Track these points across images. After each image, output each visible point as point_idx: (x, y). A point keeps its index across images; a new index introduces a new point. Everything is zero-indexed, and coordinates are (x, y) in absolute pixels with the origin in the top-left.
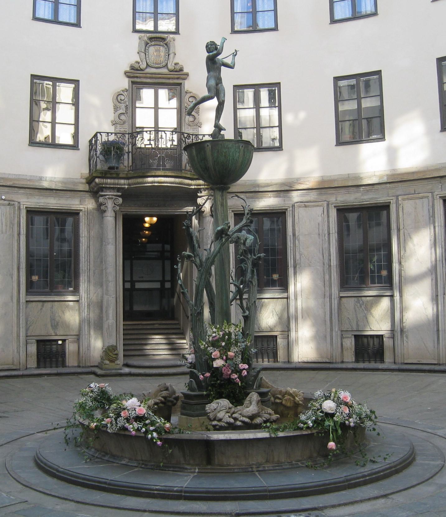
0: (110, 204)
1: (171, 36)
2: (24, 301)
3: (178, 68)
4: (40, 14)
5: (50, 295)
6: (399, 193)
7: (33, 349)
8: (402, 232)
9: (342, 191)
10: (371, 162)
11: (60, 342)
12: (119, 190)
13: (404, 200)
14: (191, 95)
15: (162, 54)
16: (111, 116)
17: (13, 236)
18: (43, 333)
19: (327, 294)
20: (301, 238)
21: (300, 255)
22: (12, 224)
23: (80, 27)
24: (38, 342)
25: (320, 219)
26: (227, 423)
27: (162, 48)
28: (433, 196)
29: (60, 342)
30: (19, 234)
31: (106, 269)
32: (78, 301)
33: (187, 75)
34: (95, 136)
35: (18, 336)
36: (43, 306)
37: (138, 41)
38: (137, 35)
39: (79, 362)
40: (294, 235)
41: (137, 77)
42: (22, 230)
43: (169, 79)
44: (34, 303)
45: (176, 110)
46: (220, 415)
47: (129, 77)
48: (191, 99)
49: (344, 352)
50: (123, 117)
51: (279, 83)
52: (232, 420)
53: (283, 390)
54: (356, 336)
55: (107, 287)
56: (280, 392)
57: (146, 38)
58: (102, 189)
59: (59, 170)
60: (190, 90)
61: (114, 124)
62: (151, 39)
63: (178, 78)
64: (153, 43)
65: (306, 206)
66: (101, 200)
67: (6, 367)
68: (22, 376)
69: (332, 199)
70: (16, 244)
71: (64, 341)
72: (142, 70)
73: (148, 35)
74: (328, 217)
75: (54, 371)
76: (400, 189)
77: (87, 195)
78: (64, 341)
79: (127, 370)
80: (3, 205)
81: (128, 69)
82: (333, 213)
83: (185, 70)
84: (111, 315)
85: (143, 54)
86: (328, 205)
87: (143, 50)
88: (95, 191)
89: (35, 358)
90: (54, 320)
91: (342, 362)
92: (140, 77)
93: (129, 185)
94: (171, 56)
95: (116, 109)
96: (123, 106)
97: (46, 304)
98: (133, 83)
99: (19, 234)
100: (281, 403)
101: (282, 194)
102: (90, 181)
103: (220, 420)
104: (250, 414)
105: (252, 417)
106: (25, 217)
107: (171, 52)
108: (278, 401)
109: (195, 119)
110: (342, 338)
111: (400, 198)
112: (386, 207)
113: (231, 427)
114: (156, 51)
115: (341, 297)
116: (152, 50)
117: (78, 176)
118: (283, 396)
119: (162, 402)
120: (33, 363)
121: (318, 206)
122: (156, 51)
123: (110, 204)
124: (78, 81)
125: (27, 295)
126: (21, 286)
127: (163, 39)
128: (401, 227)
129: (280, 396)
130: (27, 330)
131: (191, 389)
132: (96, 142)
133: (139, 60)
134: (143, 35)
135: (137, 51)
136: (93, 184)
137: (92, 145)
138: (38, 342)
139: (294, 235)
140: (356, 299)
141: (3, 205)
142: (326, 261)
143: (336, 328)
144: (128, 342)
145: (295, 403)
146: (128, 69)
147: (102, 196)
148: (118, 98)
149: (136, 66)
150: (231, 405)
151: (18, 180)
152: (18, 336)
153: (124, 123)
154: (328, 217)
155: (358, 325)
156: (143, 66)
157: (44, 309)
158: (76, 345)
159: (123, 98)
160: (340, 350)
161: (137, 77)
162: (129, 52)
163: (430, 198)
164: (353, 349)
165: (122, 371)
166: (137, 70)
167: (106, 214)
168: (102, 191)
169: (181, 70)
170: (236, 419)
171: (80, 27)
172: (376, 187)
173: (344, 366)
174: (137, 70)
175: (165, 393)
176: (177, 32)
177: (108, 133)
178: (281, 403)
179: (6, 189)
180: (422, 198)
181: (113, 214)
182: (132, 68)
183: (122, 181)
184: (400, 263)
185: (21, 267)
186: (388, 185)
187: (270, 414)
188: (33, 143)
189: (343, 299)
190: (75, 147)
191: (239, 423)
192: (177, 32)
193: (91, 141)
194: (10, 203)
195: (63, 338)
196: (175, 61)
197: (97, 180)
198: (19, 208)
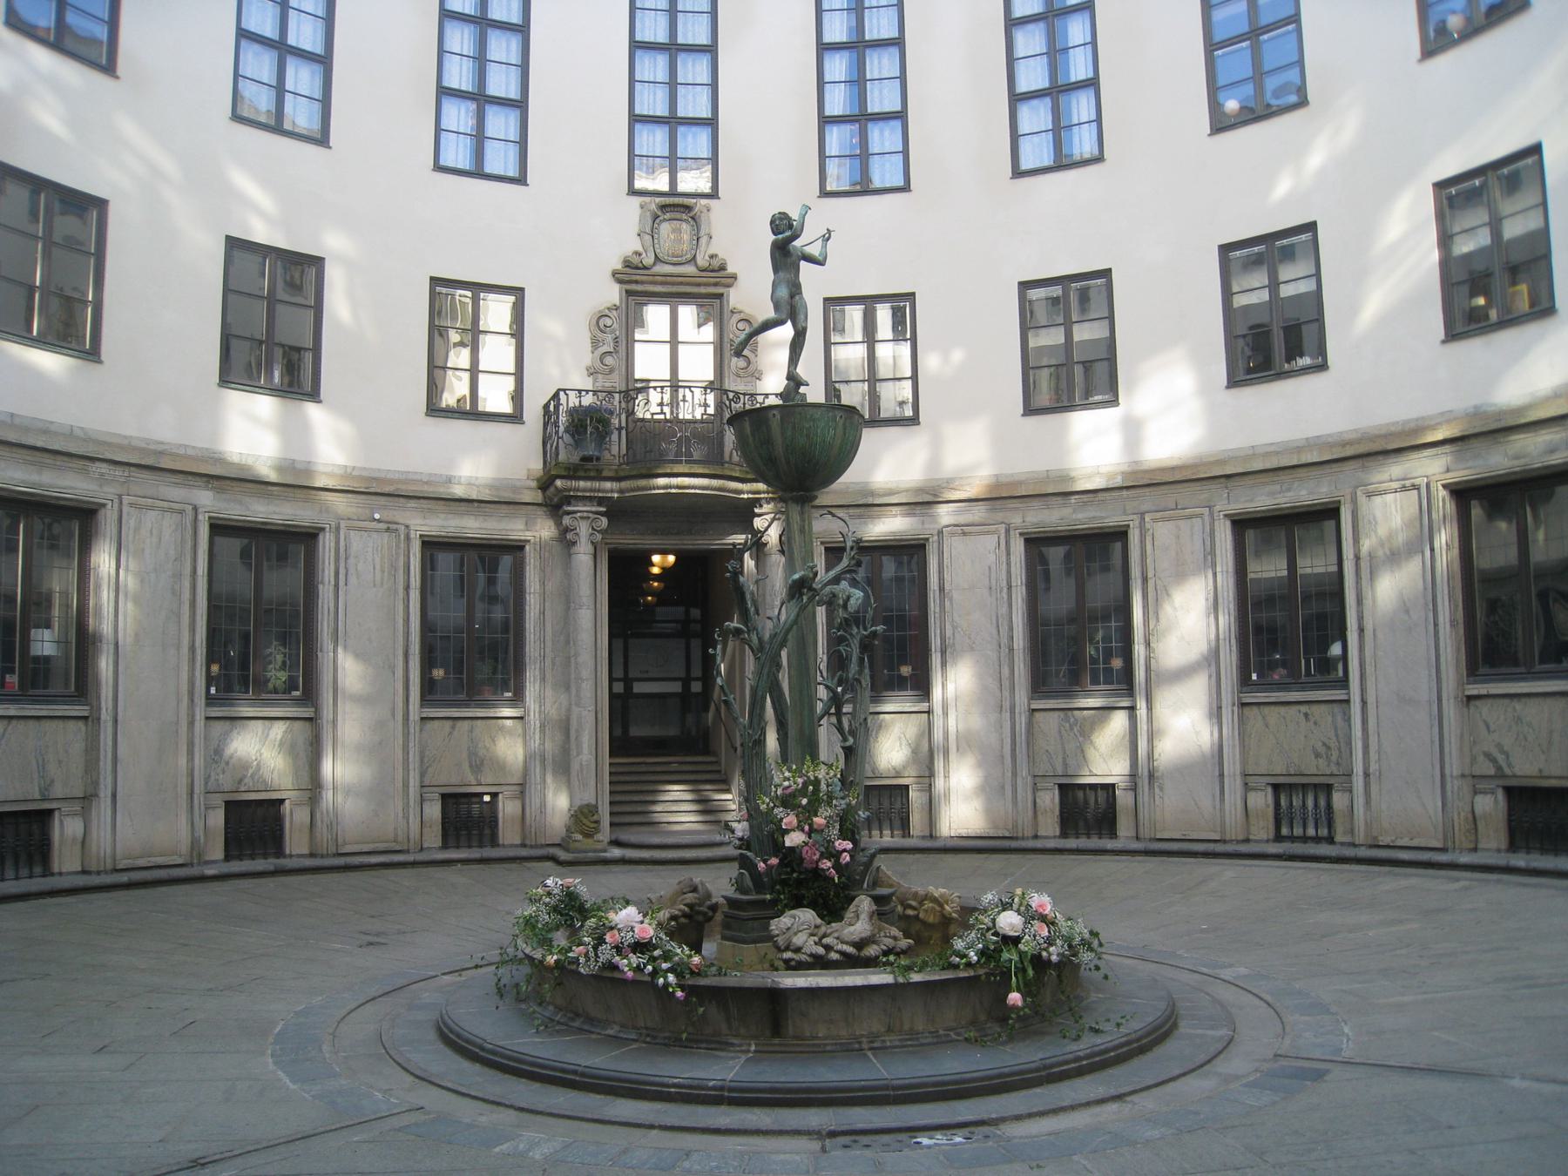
0: (584, 529)
1: (704, 202)
2: (417, 718)
3: (716, 263)
4: (448, 159)
5: (468, 706)
6: (1144, 507)
7: (434, 810)
8: (1151, 584)
9: (1036, 503)
10: (1093, 446)
11: (487, 798)
12: (600, 501)
13: (1154, 520)
14: (742, 316)
15: (686, 237)
16: (587, 358)
17: (396, 592)
18: (454, 781)
19: (1007, 705)
20: (955, 595)
21: (954, 628)
22: (394, 567)
23: (100, 362)
24: (444, 797)
25: (992, 557)
26: (811, 955)
27: (684, 226)
28: (1211, 514)
29: (487, 798)
30: (407, 588)
31: (576, 655)
32: (521, 718)
33: (734, 277)
34: (556, 396)
35: (406, 785)
36: (453, 727)
37: (638, 211)
38: (637, 200)
39: (524, 837)
40: (942, 589)
41: (636, 282)
42: (412, 579)
43: (699, 285)
44: (436, 723)
45: (711, 347)
46: (799, 940)
47: (620, 282)
48: (741, 326)
49: (1040, 817)
50: (609, 360)
51: (913, 294)
52: (821, 951)
53: (921, 891)
54: (1061, 786)
55: (578, 690)
56: (915, 895)
57: (653, 207)
58: (568, 500)
59: (487, 461)
60: (740, 307)
61: (592, 372)
62: (663, 207)
63: (716, 285)
64: (668, 216)
65: (964, 534)
66: (566, 520)
67: (381, 847)
68: (414, 864)
69: (1016, 520)
70: (401, 608)
71: (494, 795)
72: (645, 268)
73: (658, 200)
74: (1008, 554)
75: (475, 853)
76: (1148, 500)
77: (540, 511)
78: (494, 795)
79: (616, 852)
80: (377, 531)
81: (619, 267)
82: (1018, 547)
83: (731, 269)
84: (585, 746)
85: (648, 238)
86: (1007, 531)
87: (648, 230)
88: (555, 505)
89: (438, 828)
90: (476, 754)
91: (1036, 837)
92: (642, 283)
93: (621, 491)
94: (703, 240)
95: (595, 344)
96: (609, 338)
97: (459, 724)
98: (629, 293)
99: (407, 588)
100: (917, 917)
101: (918, 510)
102: (545, 484)
103: (798, 950)
104: (856, 938)
105: (860, 945)
106: (418, 555)
107: (702, 233)
108: (910, 912)
109: (749, 362)
110: (1035, 789)
111: (1147, 518)
112: (1121, 534)
113: (819, 963)
114: (674, 231)
115: (1244, 705)
116: (665, 228)
117: (522, 475)
118: (921, 903)
119: (685, 915)
120: (434, 838)
121: (988, 533)
122: (674, 231)
123: (584, 529)
124: (522, 290)
125: (422, 706)
126: (411, 688)
127: (688, 208)
128: (1150, 575)
129: (913, 903)
130: (422, 775)
131: (741, 889)
132: (557, 407)
133: (640, 249)
134: (647, 199)
135: (636, 230)
136: (552, 489)
137: (549, 414)
138: (444, 797)
139: (942, 589)
140: (1061, 714)
141: (377, 531)
142: (1004, 641)
143: (1023, 771)
144: (618, 798)
145: (943, 916)
146: (619, 267)
147: (568, 513)
148: (599, 322)
149: (636, 260)
150: (819, 921)
151: (406, 482)
152: (406, 785)
153: (611, 371)
154: (1008, 554)
155: (1065, 765)
156: (649, 260)
157: (455, 732)
158: (518, 804)
159: (608, 322)
160: (1030, 813)
161: (636, 282)
162: (619, 233)
163: (1207, 518)
164: (1057, 812)
165: (608, 855)
166: (637, 268)
167: (575, 549)
168: (569, 504)
169: (722, 268)
170: (828, 948)
171: (100, 362)
172: (1101, 496)
173: (1039, 844)
174: (637, 268)
175: (690, 898)
176: (714, 195)
177: (580, 391)
178: (917, 917)
179: (382, 500)
180: (1190, 517)
181: (590, 549)
182: (627, 264)
183: (608, 485)
184: (1148, 644)
185: (411, 651)
186: (1125, 493)
187: (895, 938)
188: (434, 409)
189: (1037, 715)
190: (516, 417)
191: (834, 956)
192: (714, 195)
193: (546, 406)
194: (390, 528)
195: (493, 789)
196: (711, 251)
197: (559, 483)
198: (408, 538)
